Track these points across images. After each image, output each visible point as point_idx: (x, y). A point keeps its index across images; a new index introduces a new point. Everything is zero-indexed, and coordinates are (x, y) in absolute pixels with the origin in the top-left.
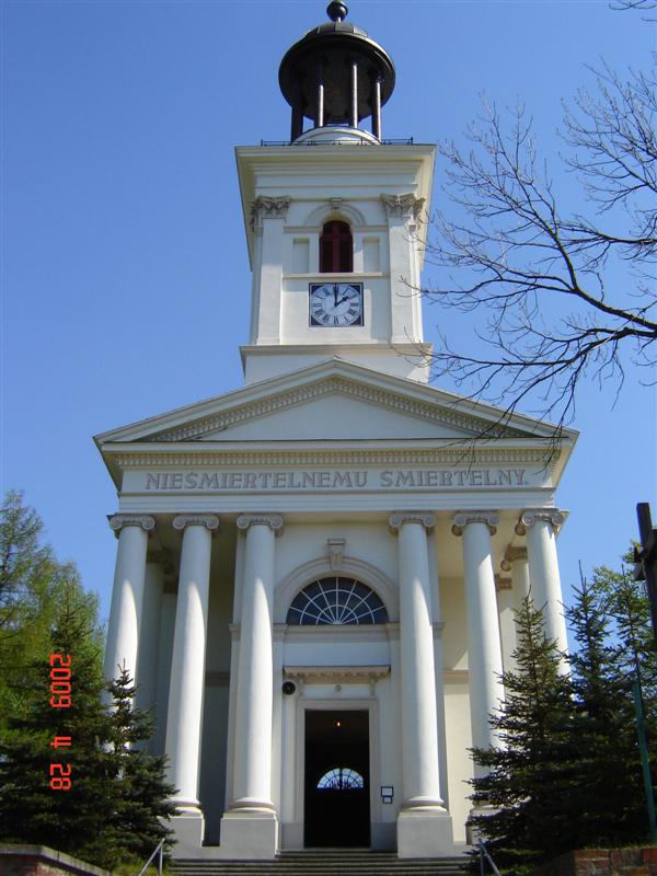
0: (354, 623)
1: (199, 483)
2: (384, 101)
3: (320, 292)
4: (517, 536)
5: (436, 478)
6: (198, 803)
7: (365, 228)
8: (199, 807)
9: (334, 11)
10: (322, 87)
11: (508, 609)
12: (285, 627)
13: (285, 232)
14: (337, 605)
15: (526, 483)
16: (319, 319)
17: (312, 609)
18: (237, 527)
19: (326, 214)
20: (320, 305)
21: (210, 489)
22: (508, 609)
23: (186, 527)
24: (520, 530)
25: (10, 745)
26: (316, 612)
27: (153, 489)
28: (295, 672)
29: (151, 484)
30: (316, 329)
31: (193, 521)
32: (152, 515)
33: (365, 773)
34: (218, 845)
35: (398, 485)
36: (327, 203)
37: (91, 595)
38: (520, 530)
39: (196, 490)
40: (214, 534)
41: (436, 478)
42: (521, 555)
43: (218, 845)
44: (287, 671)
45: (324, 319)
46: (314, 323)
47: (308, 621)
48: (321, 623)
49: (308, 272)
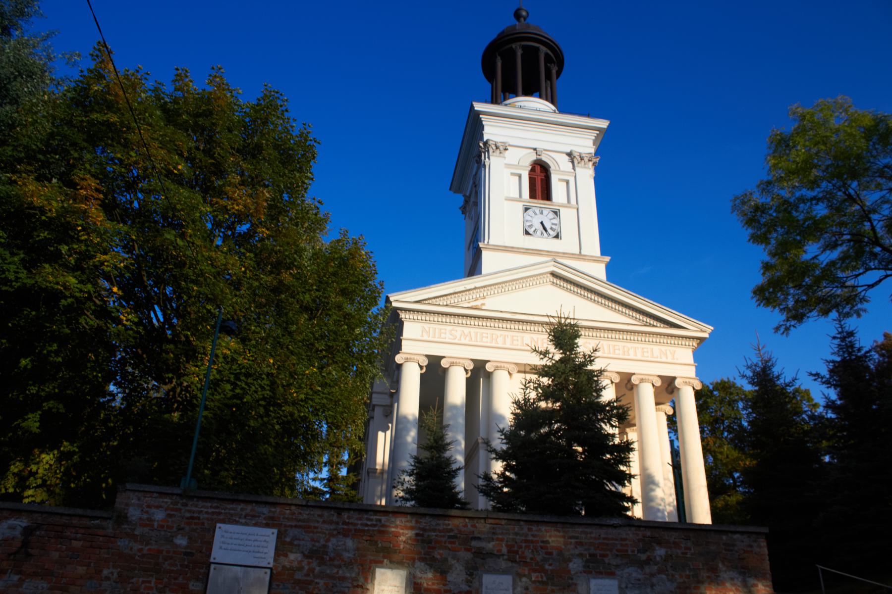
1: (458, 337)
2: (558, 77)
3: (530, 212)
5: (648, 352)
7: (559, 171)
9: (517, 15)
13: (506, 168)
15: (677, 359)
16: (531, 231)
19: (534, 157)
20: (531, 221)
21: (467, 342)
25: (65, 288)
27: (426, 338)
29: (424, 333)
30: (563, 235)
31: (501, 367)
35: (460, 340)
36: (532, 151)
38: (629, 386)
39: (456, 341)
41: (648, 352)
45: (534, 231)
46: (527, 233)
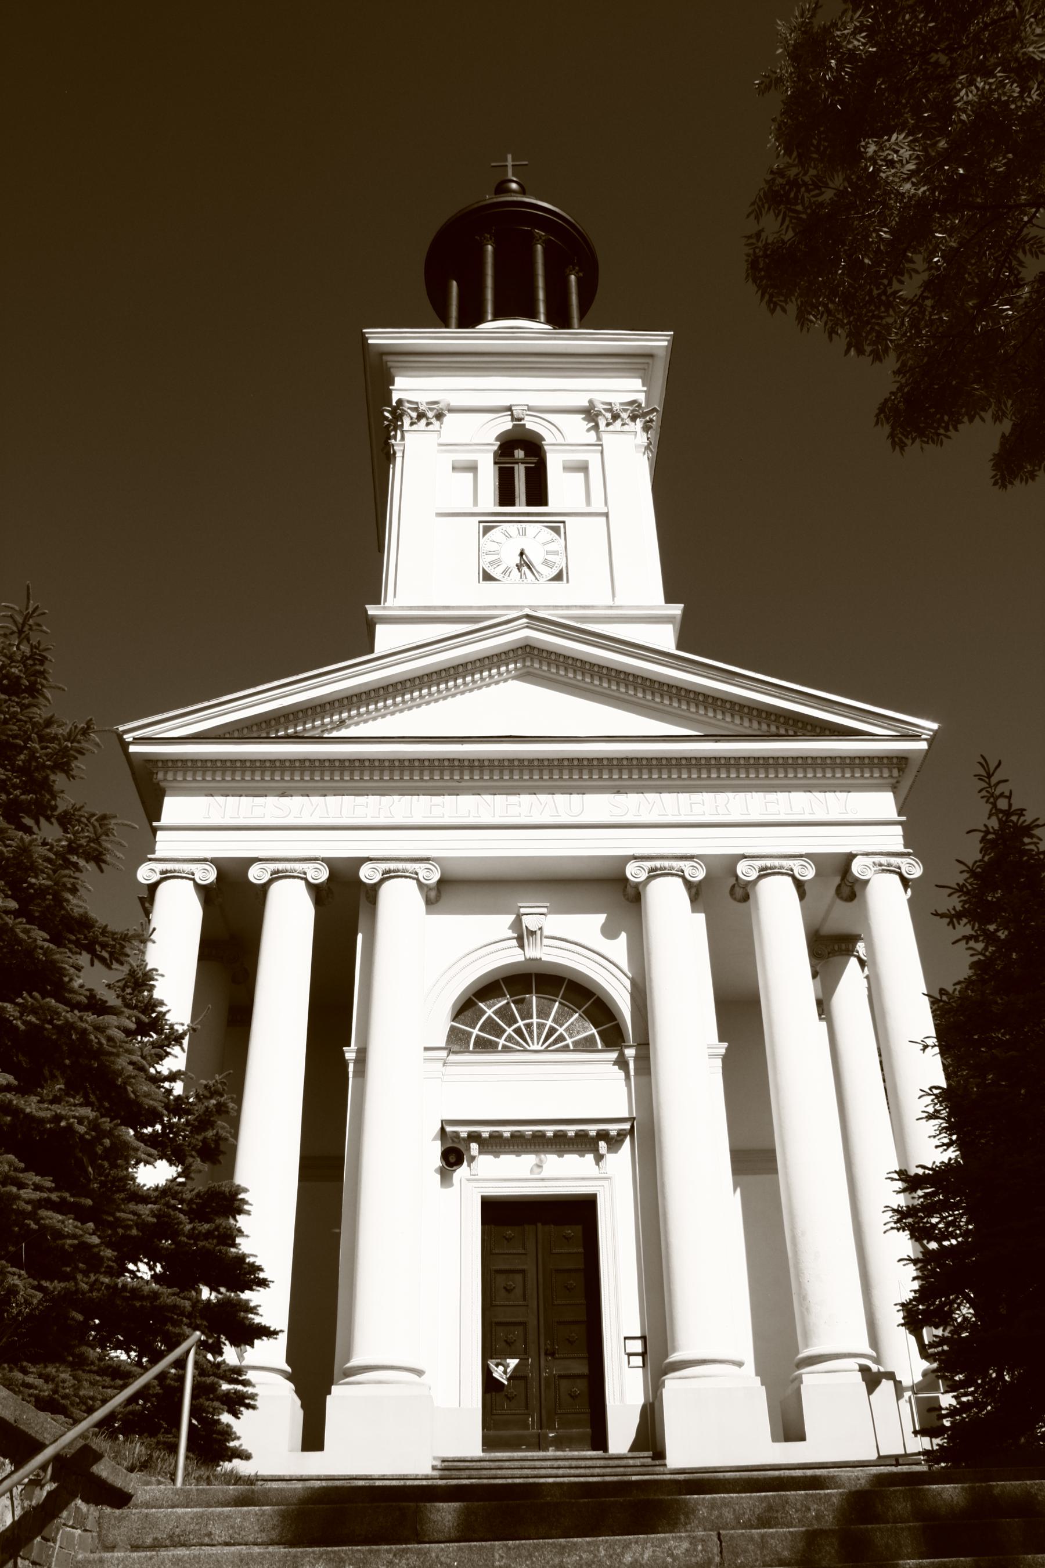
0: (566, 1049)
4: (839, 902)
6: (289, 1369)
8: (290, 1377)
10: (454, 283)
11: (183, 1068)
12: (444, 1054)
14: (535, 1020)
16: (495, 573)
17: (491, 1027)
18: (627, 880)
20: (495, 553)
22: (183, 1068)
23: (382, 881)
24: (739, 892)
26: (499, 1032)
28: (463, 1131)
32: (214, 861)
33: (487, 1373)
34: (802, 1438)
37: (970, 968)
38: (846, 891)
40: (318, 893)
42: (844, 946)
43: (802, 1438)
44: (449, 1129)
47: (484, 1046)
48: (506, 1049)
49: (513, 504)
